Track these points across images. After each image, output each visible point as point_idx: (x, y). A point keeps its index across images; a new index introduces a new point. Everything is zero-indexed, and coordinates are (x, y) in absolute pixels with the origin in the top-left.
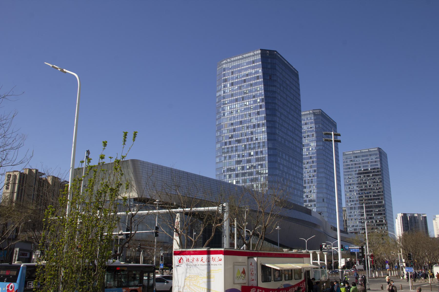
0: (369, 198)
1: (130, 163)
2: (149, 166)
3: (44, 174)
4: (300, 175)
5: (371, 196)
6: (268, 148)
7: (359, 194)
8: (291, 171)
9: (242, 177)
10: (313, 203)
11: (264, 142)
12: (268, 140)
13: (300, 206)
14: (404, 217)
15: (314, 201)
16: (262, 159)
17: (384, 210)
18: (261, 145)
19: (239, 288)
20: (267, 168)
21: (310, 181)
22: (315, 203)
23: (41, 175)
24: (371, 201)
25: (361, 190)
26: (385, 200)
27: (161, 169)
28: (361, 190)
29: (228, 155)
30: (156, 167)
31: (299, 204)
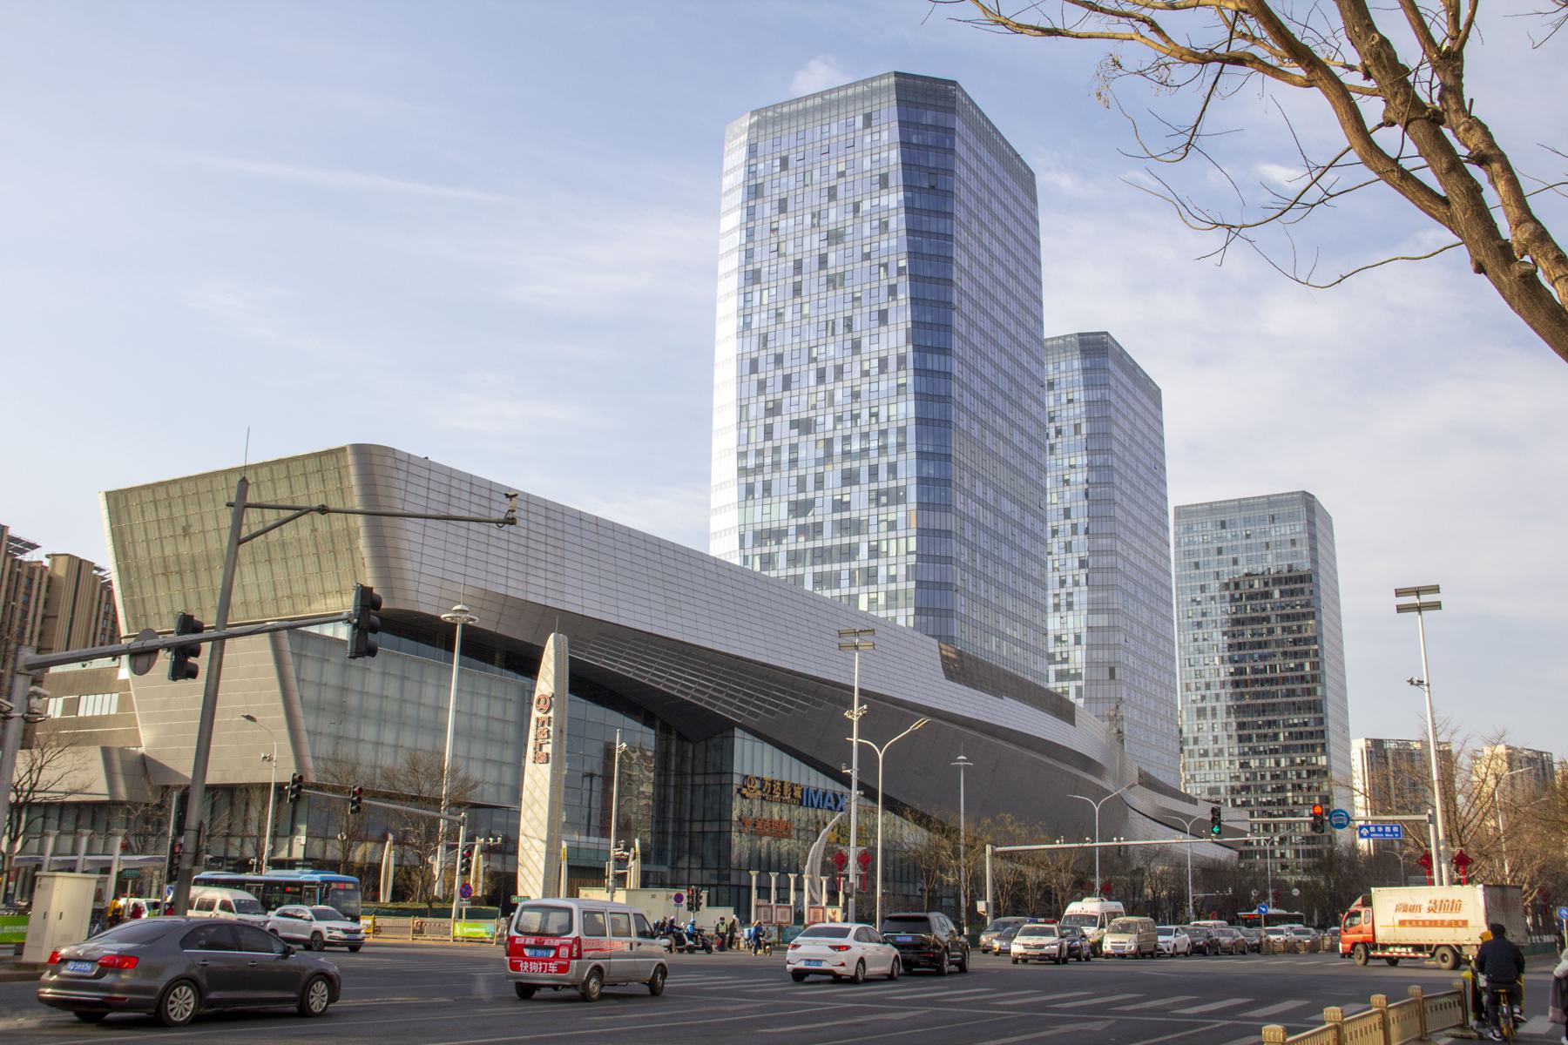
0: (1268, 675)
1: (351, 459)
2: (434, 476)
3: (34, 546)
4: (1037, 567)
5: (1273, 668)
6: (921, 455)
7: (1231, 660)
8: (1005, 548)
9: (813, 564)
10: (1072, 683)
11: (902, 431)
12: (920, 420)
13: (1037, 687)
14: (1377, 750)
15: (1077, 676)
16: (896, 497)
17: (1321, 721)
18: (892, 440)
19: (514, 899)
20: (914, 532)
21: (1063, 602)
22: (1079, 683)
23: (23, 552)
24: (1274, 688)
25: (1240, 646)
26: (1324, 686)
27: (485, 493)
28: (1240, 646)
29: (759, 478)
30: (466, 487)
31: (1029, 678)
